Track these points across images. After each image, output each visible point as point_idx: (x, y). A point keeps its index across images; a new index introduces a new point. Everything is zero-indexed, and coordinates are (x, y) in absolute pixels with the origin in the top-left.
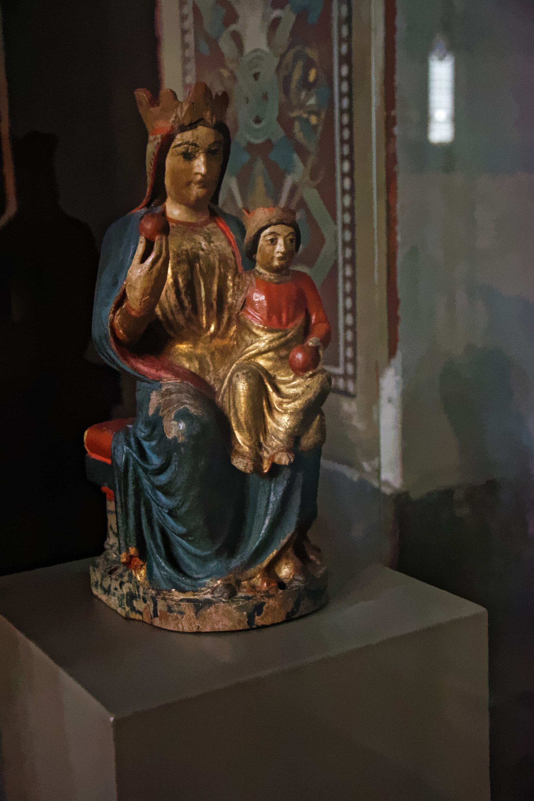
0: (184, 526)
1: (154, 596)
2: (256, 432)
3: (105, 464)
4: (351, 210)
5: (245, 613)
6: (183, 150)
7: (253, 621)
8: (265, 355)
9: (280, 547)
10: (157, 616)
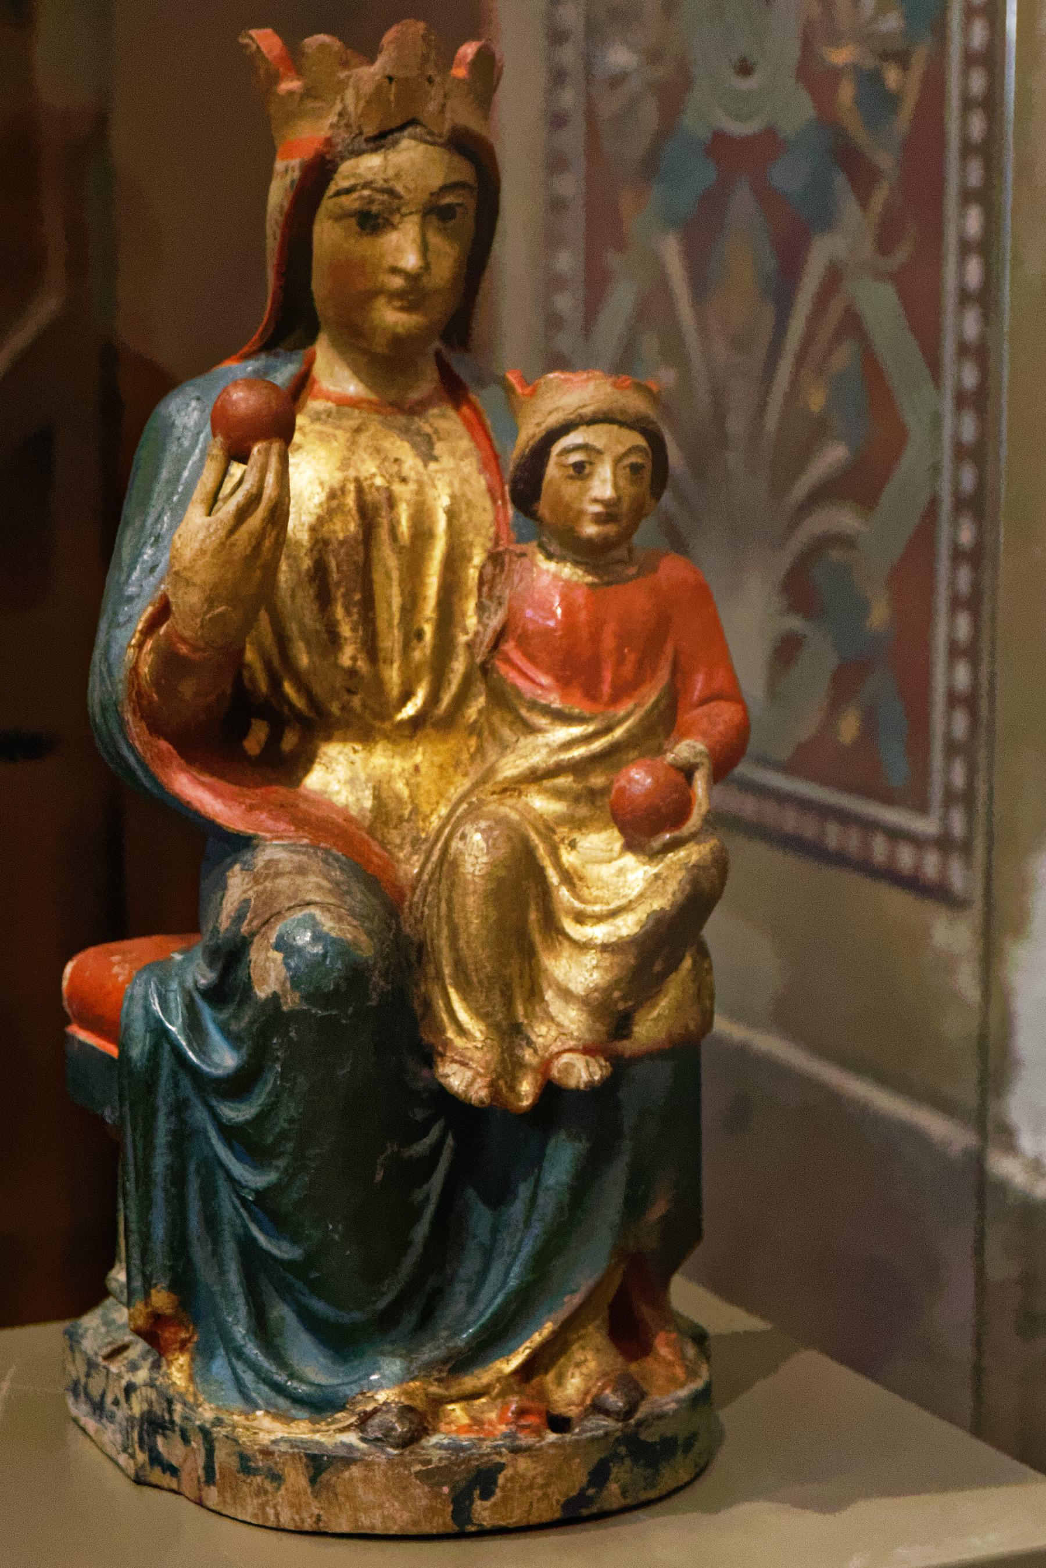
0: (295, 1240)
1: (208, 1426)
2: (503, 994)
3: (104, 1056)
4: (980, 353)
5: (446, 1490)
6: (356, 205)
7: (469, 1509)
8: (548, 783)
9: (563, 1314)
10: (214, 1484)
